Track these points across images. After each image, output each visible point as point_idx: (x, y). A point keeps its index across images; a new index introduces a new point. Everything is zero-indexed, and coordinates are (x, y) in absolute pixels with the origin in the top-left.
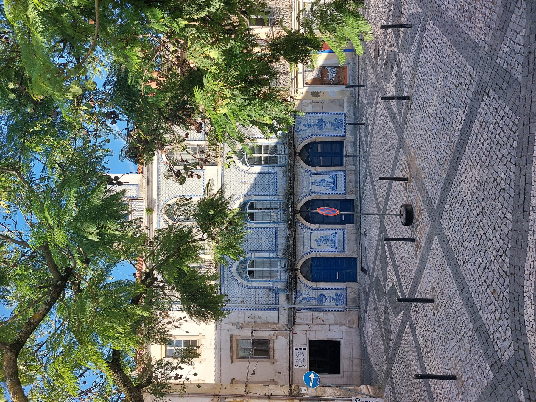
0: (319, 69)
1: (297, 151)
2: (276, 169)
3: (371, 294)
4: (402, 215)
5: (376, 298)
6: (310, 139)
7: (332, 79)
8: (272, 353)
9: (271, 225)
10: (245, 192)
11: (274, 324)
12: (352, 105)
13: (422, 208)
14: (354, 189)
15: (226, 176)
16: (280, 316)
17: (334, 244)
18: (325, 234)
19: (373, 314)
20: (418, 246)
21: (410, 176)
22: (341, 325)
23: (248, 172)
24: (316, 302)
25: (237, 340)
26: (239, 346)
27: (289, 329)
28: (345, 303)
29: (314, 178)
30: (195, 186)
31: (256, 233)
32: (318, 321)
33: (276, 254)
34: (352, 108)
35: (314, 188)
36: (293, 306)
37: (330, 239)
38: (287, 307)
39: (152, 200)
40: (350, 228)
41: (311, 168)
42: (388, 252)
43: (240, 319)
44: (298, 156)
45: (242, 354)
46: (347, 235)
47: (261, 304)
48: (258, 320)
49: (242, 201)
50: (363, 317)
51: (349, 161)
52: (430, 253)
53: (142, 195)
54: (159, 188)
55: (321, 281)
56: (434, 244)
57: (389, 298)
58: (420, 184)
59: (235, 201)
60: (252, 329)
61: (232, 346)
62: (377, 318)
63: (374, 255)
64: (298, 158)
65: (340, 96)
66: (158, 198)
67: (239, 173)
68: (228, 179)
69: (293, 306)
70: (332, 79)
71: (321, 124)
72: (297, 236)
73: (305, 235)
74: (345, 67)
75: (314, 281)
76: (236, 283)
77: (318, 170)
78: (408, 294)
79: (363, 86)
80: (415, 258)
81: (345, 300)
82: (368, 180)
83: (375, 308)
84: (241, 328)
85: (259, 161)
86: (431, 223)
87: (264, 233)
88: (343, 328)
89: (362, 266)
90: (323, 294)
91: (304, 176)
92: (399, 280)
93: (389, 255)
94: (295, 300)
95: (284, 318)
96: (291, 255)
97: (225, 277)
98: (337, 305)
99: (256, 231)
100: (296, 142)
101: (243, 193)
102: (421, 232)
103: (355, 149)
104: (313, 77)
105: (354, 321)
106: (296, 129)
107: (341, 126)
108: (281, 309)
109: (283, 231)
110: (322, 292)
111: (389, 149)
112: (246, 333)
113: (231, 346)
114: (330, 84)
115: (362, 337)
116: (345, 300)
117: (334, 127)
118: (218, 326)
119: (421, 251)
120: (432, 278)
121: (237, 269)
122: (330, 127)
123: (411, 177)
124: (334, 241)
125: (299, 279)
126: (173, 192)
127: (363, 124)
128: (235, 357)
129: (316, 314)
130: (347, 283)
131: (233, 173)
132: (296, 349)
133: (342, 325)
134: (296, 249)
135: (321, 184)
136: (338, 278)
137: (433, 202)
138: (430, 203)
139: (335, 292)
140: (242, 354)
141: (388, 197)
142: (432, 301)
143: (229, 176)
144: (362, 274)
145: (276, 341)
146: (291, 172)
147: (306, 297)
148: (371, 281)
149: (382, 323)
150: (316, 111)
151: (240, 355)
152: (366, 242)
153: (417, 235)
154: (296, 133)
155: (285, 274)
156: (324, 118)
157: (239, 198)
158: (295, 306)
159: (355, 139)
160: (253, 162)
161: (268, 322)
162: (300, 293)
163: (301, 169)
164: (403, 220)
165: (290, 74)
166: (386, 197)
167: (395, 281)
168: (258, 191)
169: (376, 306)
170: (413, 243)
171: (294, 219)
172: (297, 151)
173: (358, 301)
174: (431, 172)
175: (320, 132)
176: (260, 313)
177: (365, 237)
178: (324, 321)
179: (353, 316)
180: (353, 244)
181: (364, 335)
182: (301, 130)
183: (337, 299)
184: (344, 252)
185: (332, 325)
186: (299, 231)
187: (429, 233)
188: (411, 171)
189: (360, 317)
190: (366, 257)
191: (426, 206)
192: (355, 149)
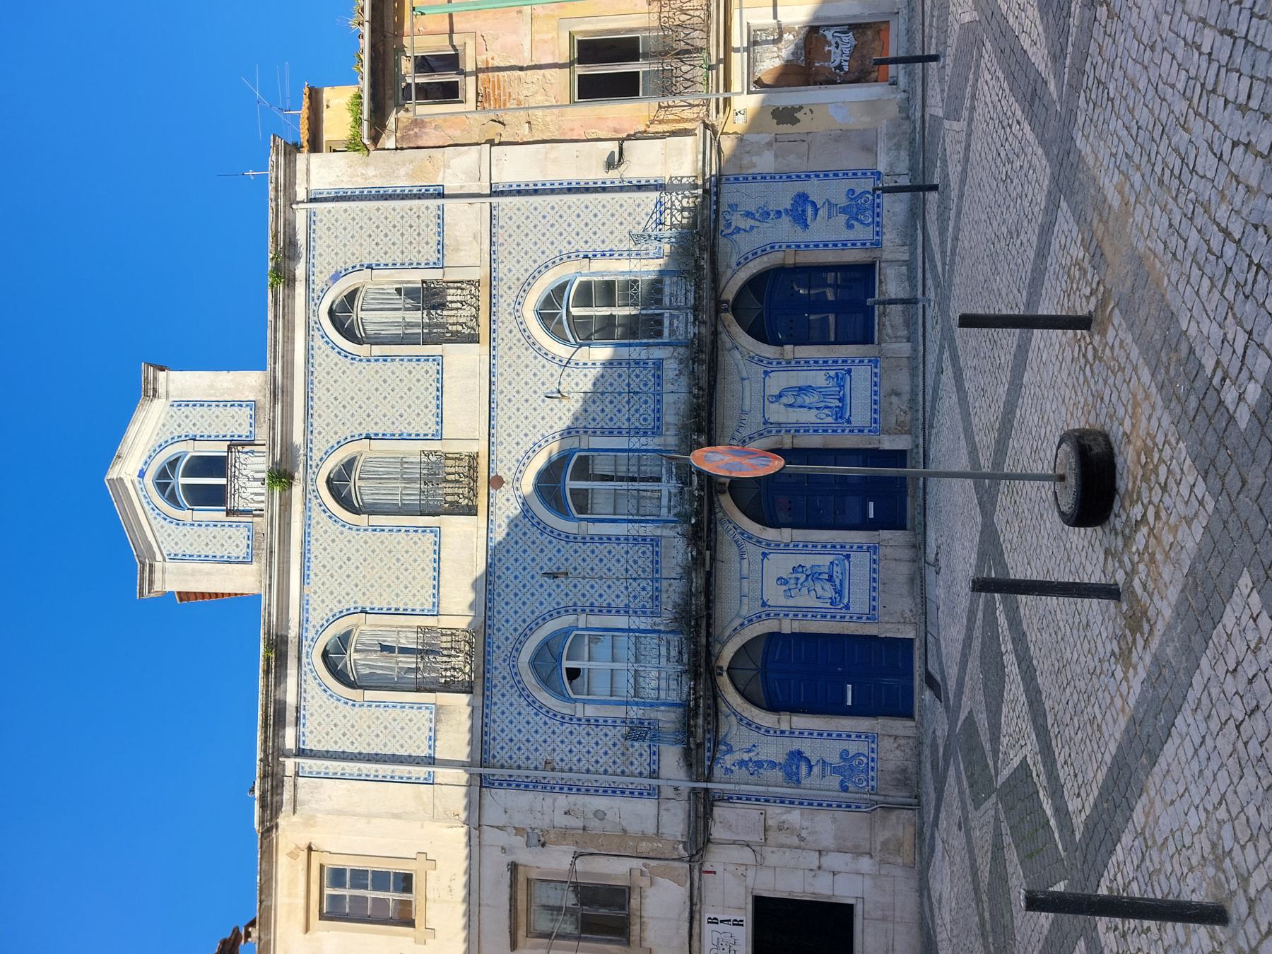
0: (798, 33)
1: (724, 297)
2: (658, 353)
3: (952, 772)
4: (1062, 478)
5: (967, 791)
6: (765, 258)
7: (840, 67)
8: (635, 929)
9: (635, 529)
10: (566, 422)
11: (644, 837)
12: (905, 144)
13: (1160, 439)
14: (909, 417)
15: (505, 375)
16: (663, 813)
17: (840, 593)
18: (809, 561)
19: (958, 840)
20: (1136, 621)
21: (1102, 304)
22: (857, 853)
23: (573, 363)
24: (778, 775)
25: (528, 880)
26: (537, 900)
27: (691, 856)
28: (871, 783)
29: (778, 381)
30: (414, 407)
31: (593, 552)
32: (783, 838)
33: (649, 620)
34: (904, 154)
35: (778, 413)
36: (703, 785)
37: (826, 576)
38: (686, 786)
39: (288, 448)
40: (892, 543)
41: (768, 351)
42: (1007, 633)
43: (539, 815)
44: (726, 310)
45: (543, 923)
46: (882, 563)
47: (606, 772)
48: (594, 824)
49: (555, 451)
50: (928, 836)
51: (892, 327)
52: (1204, 662)
53: (262, 434)
54: (310, 412)
55: (794, 710)
56: (1229, 620)
57: (1009, 809)
58: (1151, 323)
59: (530, 454)
60: (575, 848)
61: (513, 899)
62: (967, 862)
63: (961, 637)
64: (729, 317)
65: (866, 119)
66: (307, 442)
67: (544, 366)
68: (510, 384)
69: (703, 785)
70: (840, 67)
71: (801, 209)
72: (719, 564)
73: (745, 562)
74: (883, 27)
75: (772, 706)
76: (530, 704)
77: (789, 356)
78: (1086, 825)
79: (935, 58)
80: (1119, 674)
81: (871, 773)
82: (947, 377)
83: (964, 825)
84: (543, 845)
85: (606, 329)
86: (1210, 505)
87: (619, 550)
88: (865, 864)
89: (926, 669)
90: (800, 753)
91: (744, 375)
92: (1046, 750)
93: (1010, 646)
94: (711, 768)
95: (675, 822)
96: (698, 625)
97: (496, 686)
98: (845, 789)
99: (593, 547)
100: (721, 269)
101: (556, 428)
102: (1152, 555)
103: (913, 287)
104: (778, 63)
105: (901, 845)
106: (721, 228)
107: (869, 213)
108: (667, 792)
109: (677, 551)
110: (797, 744)
111: (1014, 232)
112: (557, 860)
113: (511, 899)
114: (834, 82)
115: (925, 900)
116: (871, 773)
117: (843, 218)
118: (475, 833)
119: (1154, 644)
120: (1215, 798)
121: (534, 663)
122: (829, 217)
123: (1103, 311)
124: (838, 584)
125: (726, 701)
126: (348, 424)
127: (934, 188)
128: (522, 932)
129: (776, 813)
130: (881, 721)
131: (527, 366)
132: (713, 921)
133: (862, 854)
134: (718, 605)
135: (799, 400)
136: (849, 703)
137: (1230, 396)
138: (1210, 403)
139: (839, 746)
140: (543, 923)
141: (1011, 422)
142: (1213, 915)
143: (514, 375)
144: (928, 695)
145: (650, 892)
146: (701, 362)
147: (746, 759)
148: (952, 724)
149: (984, 886)
150: (786, 169)
151: (538, 928)
152: (938, 591)
153: (1134, 571)
154: (722, 241)
155: (680, 684)
156: (814, 189)
157: (543, 443)
158: (710, 785)
159: (911, 254)
160: (586, 332)
161: (624, 830)
162: (726, 744)
163: (736, 352)
164: (1068, 501)
165: (705, 55)
166: (1003, 424)
167: (1030, 749)
168: (602, 421)
169: (966, 819)
170: (1112, 604)
171: (711, 512)
172: (724, 297)
173: (914, 777)
174: (1216, 240)
175: (799, 235)
176: (601, 802)
177: (937, 573)
178: (802, 839)
179: (899, 827)
180: (901, 595)
181: (929, 898)
182: (738, 230)
183: (847, 768)
184: (872, 619)
185: (828, 851)
186: (728, 550)
187: (1201, 557)
188: (1108, 278)
189: (920, 834)
190: (937, 640)
191: (1185, 426)
192: (913, 287)
